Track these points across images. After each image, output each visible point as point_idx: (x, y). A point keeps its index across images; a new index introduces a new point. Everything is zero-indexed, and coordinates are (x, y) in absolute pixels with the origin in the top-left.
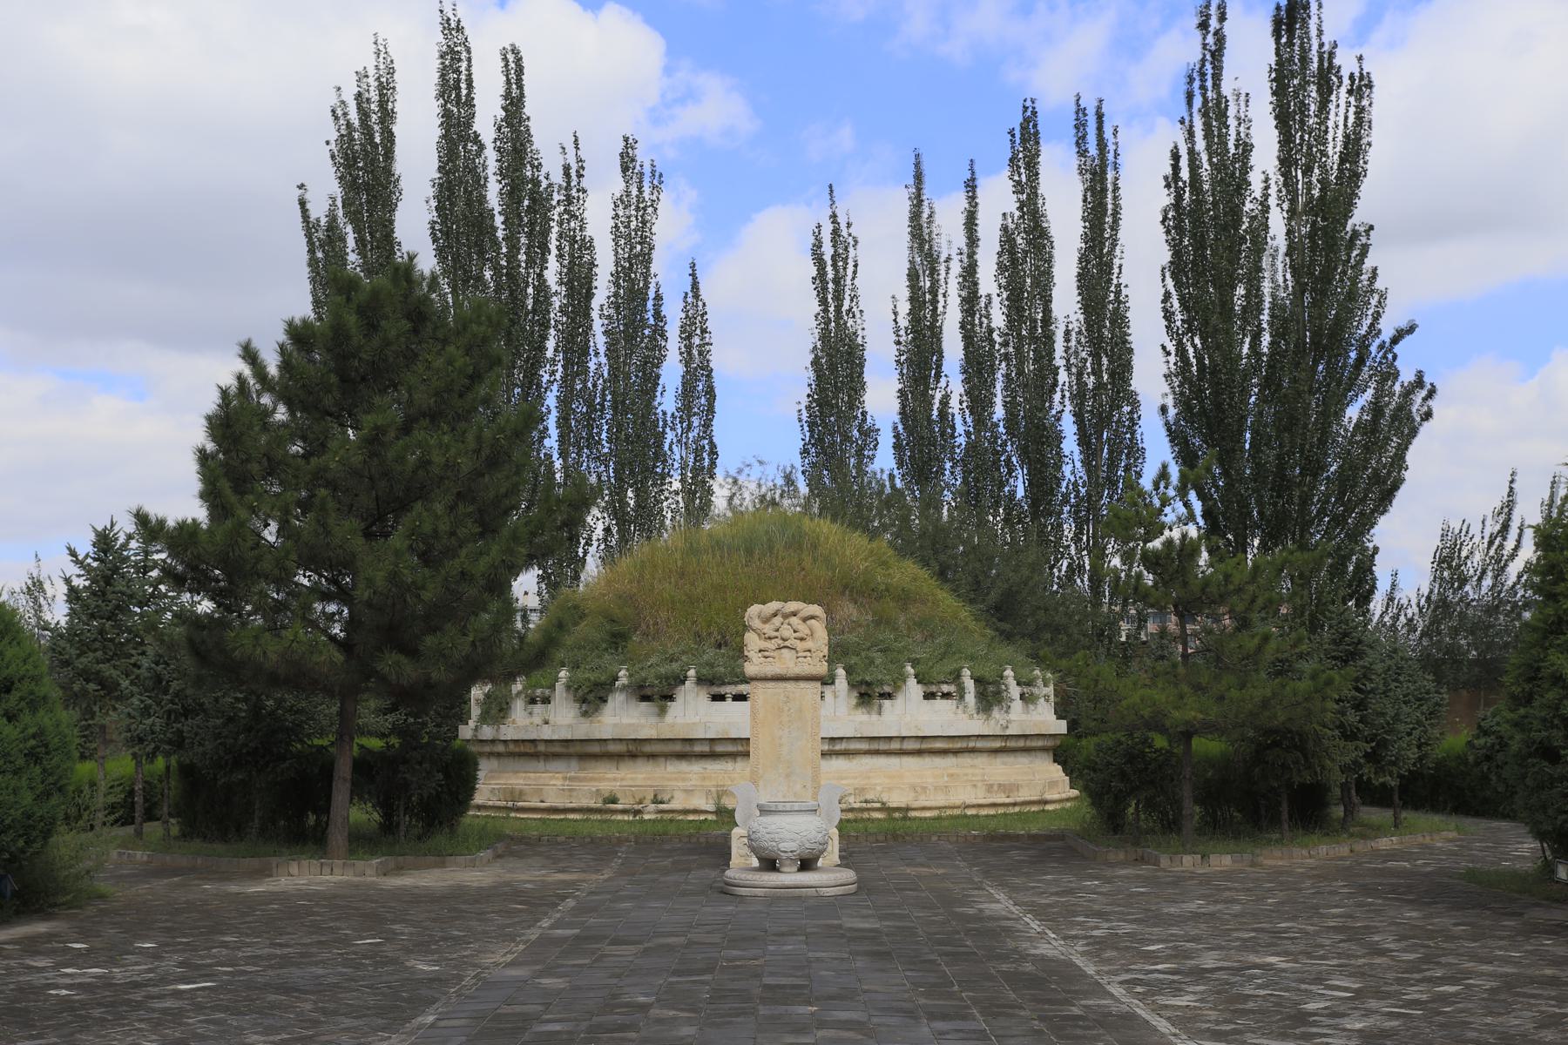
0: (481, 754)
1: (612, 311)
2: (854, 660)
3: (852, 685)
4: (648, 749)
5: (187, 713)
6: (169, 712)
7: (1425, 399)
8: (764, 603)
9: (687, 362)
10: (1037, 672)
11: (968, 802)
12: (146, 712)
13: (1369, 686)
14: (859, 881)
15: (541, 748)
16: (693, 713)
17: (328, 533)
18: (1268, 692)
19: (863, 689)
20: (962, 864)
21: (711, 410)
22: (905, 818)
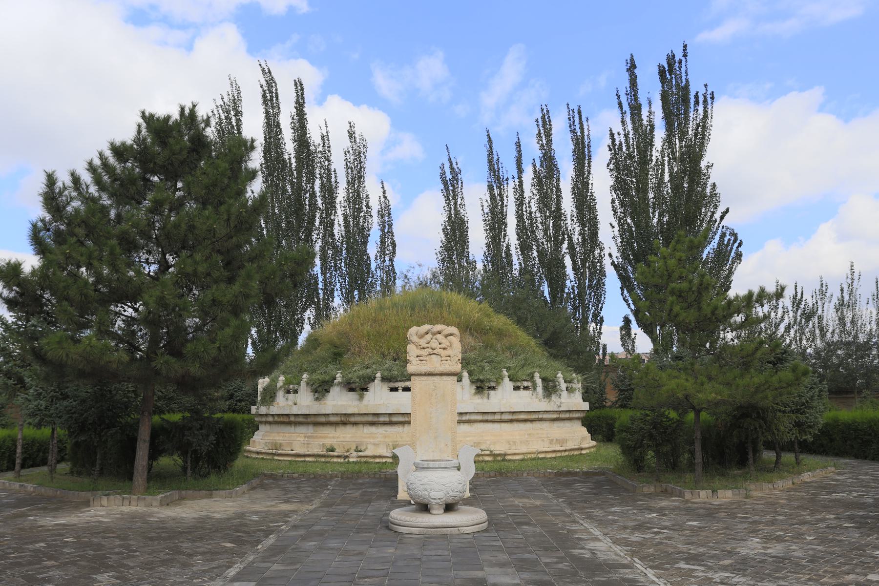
0: (261, 422)
1: (346, 204)
2: (473, 367)
3: (472, 382)
4: (352, 419)
7: (738, 247)
9: (383, 230)
10: (574, 375)
11: (540, 450)
14: (490, 521)
15: (292, 419)
16: (380, 398)
19: (479, 384)
21: (394, 253)
22: (504, 460)
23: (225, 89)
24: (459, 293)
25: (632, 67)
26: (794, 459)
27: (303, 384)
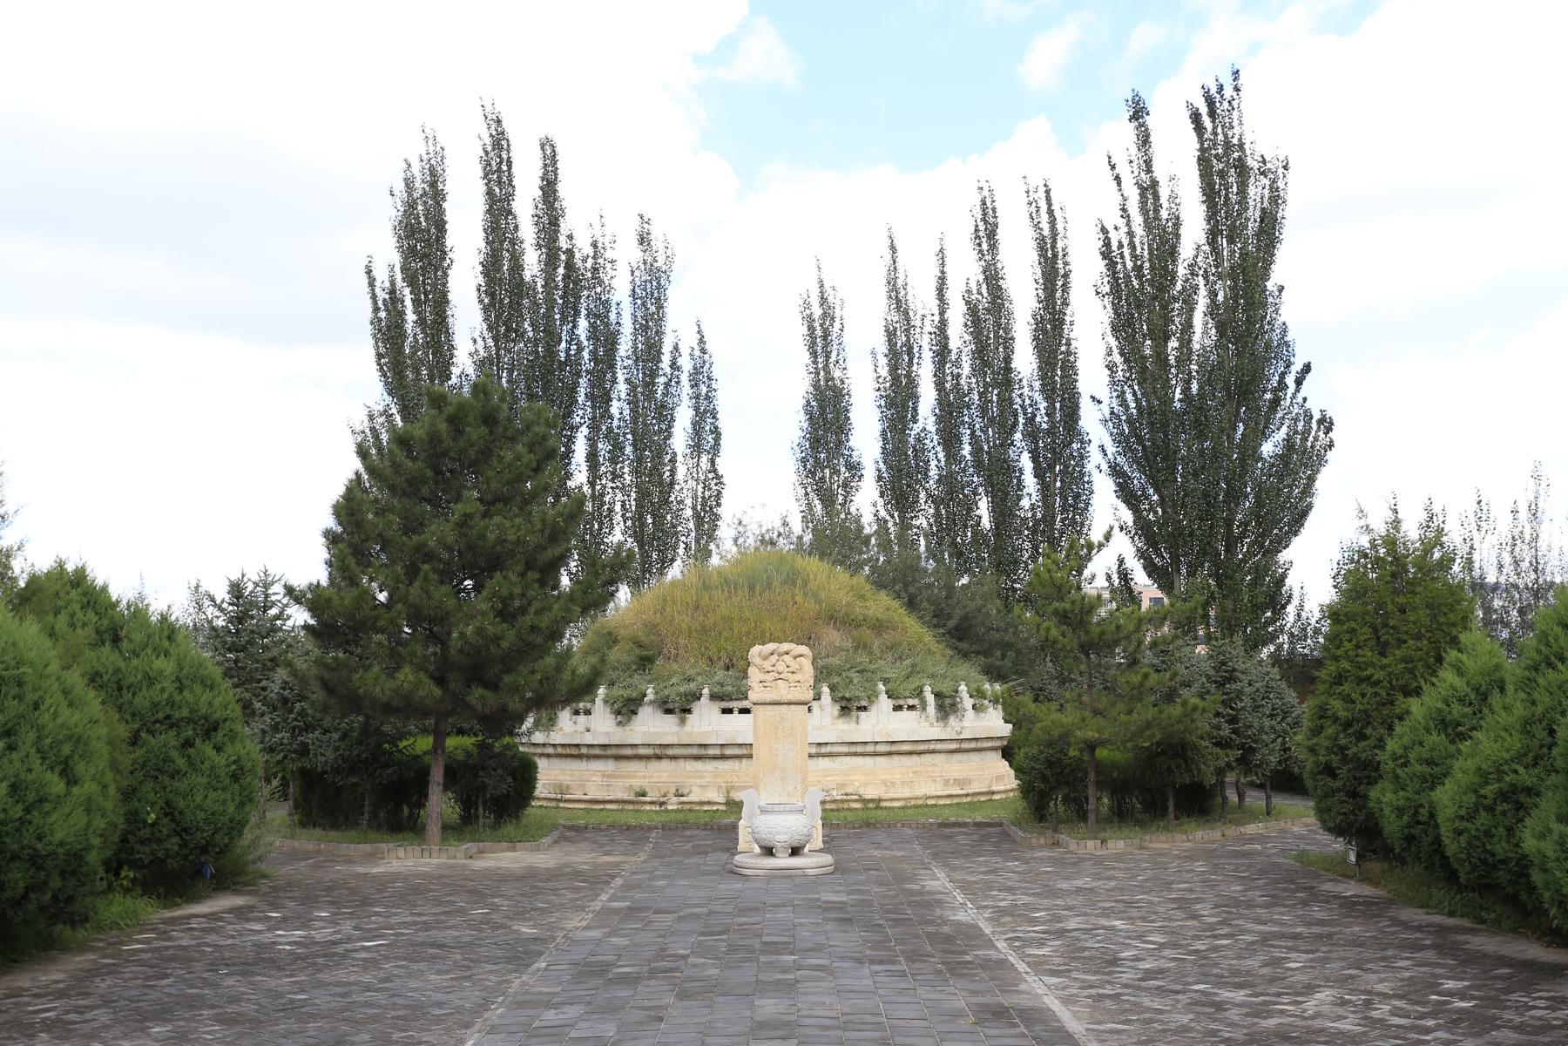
2: (836, 679)
3: (835, 700)
4: (670, 752)
5: (308, 728)
6: (294, 728)
8: (763, 644)
9: (697, 409)
12: (275, 728)
13: (1240, 705)
15: (584, 751)
16: (707, 722)
17: (429, 597)
18: (1150, 717)
19: (844, 704)
20: (918, 848)
23: (415, 150)
24: (821, 559)
25: (1138, 112)
26: (1263, 803)
27: (599, 701)
